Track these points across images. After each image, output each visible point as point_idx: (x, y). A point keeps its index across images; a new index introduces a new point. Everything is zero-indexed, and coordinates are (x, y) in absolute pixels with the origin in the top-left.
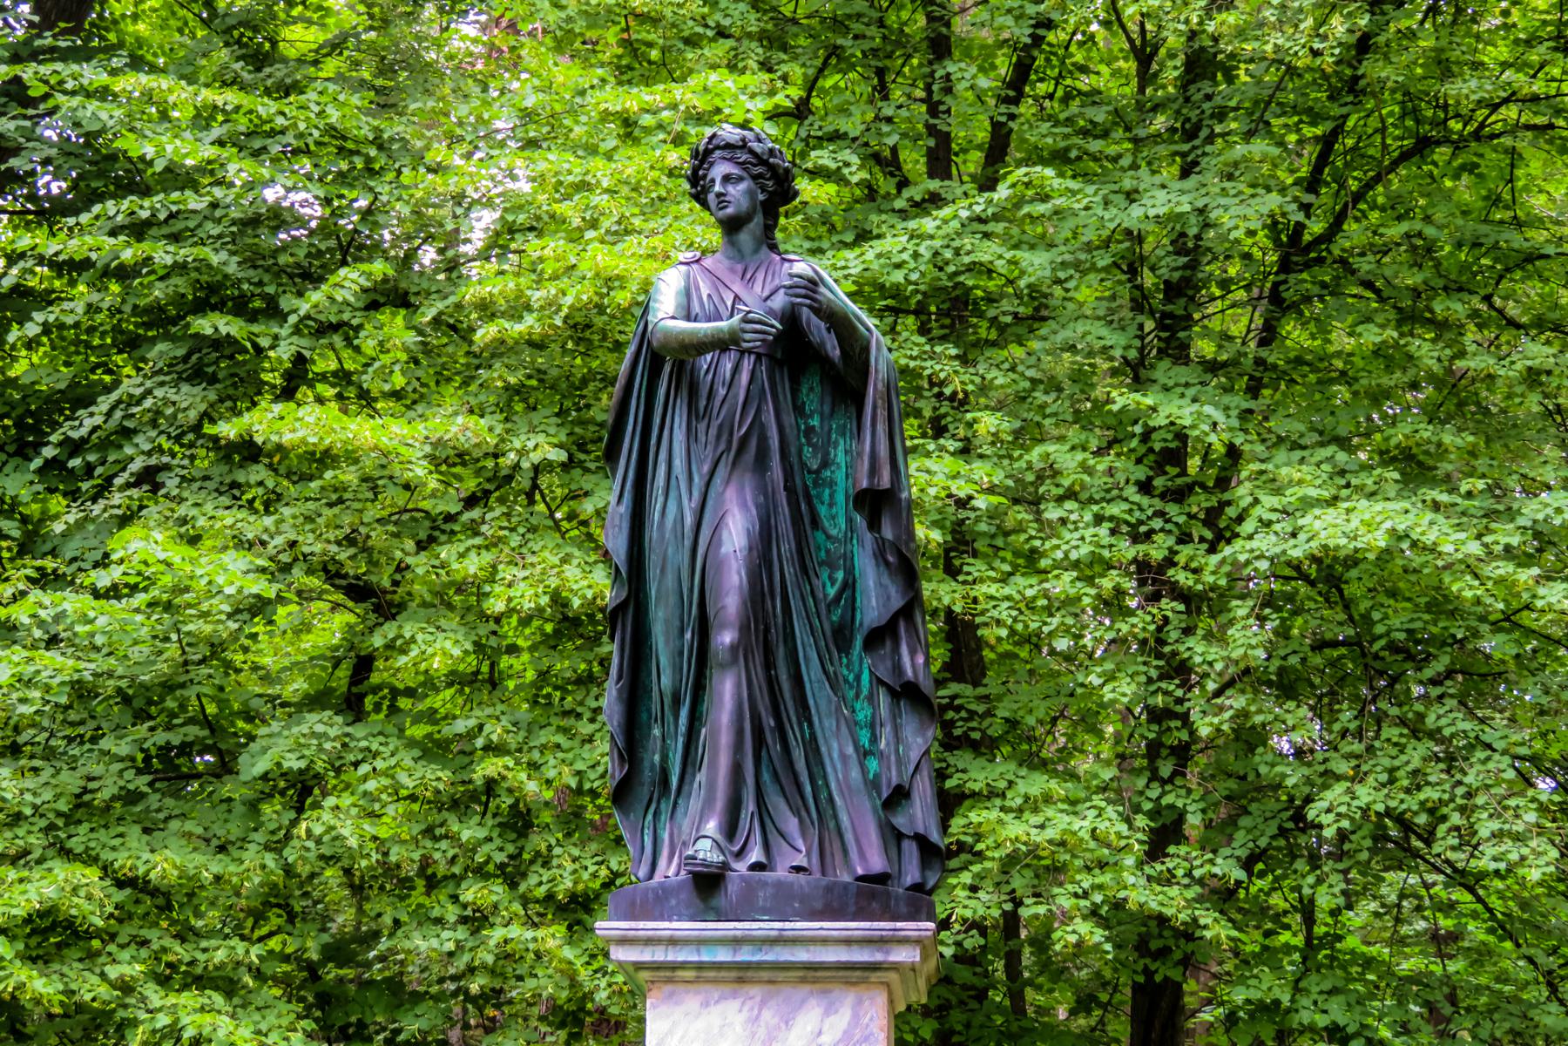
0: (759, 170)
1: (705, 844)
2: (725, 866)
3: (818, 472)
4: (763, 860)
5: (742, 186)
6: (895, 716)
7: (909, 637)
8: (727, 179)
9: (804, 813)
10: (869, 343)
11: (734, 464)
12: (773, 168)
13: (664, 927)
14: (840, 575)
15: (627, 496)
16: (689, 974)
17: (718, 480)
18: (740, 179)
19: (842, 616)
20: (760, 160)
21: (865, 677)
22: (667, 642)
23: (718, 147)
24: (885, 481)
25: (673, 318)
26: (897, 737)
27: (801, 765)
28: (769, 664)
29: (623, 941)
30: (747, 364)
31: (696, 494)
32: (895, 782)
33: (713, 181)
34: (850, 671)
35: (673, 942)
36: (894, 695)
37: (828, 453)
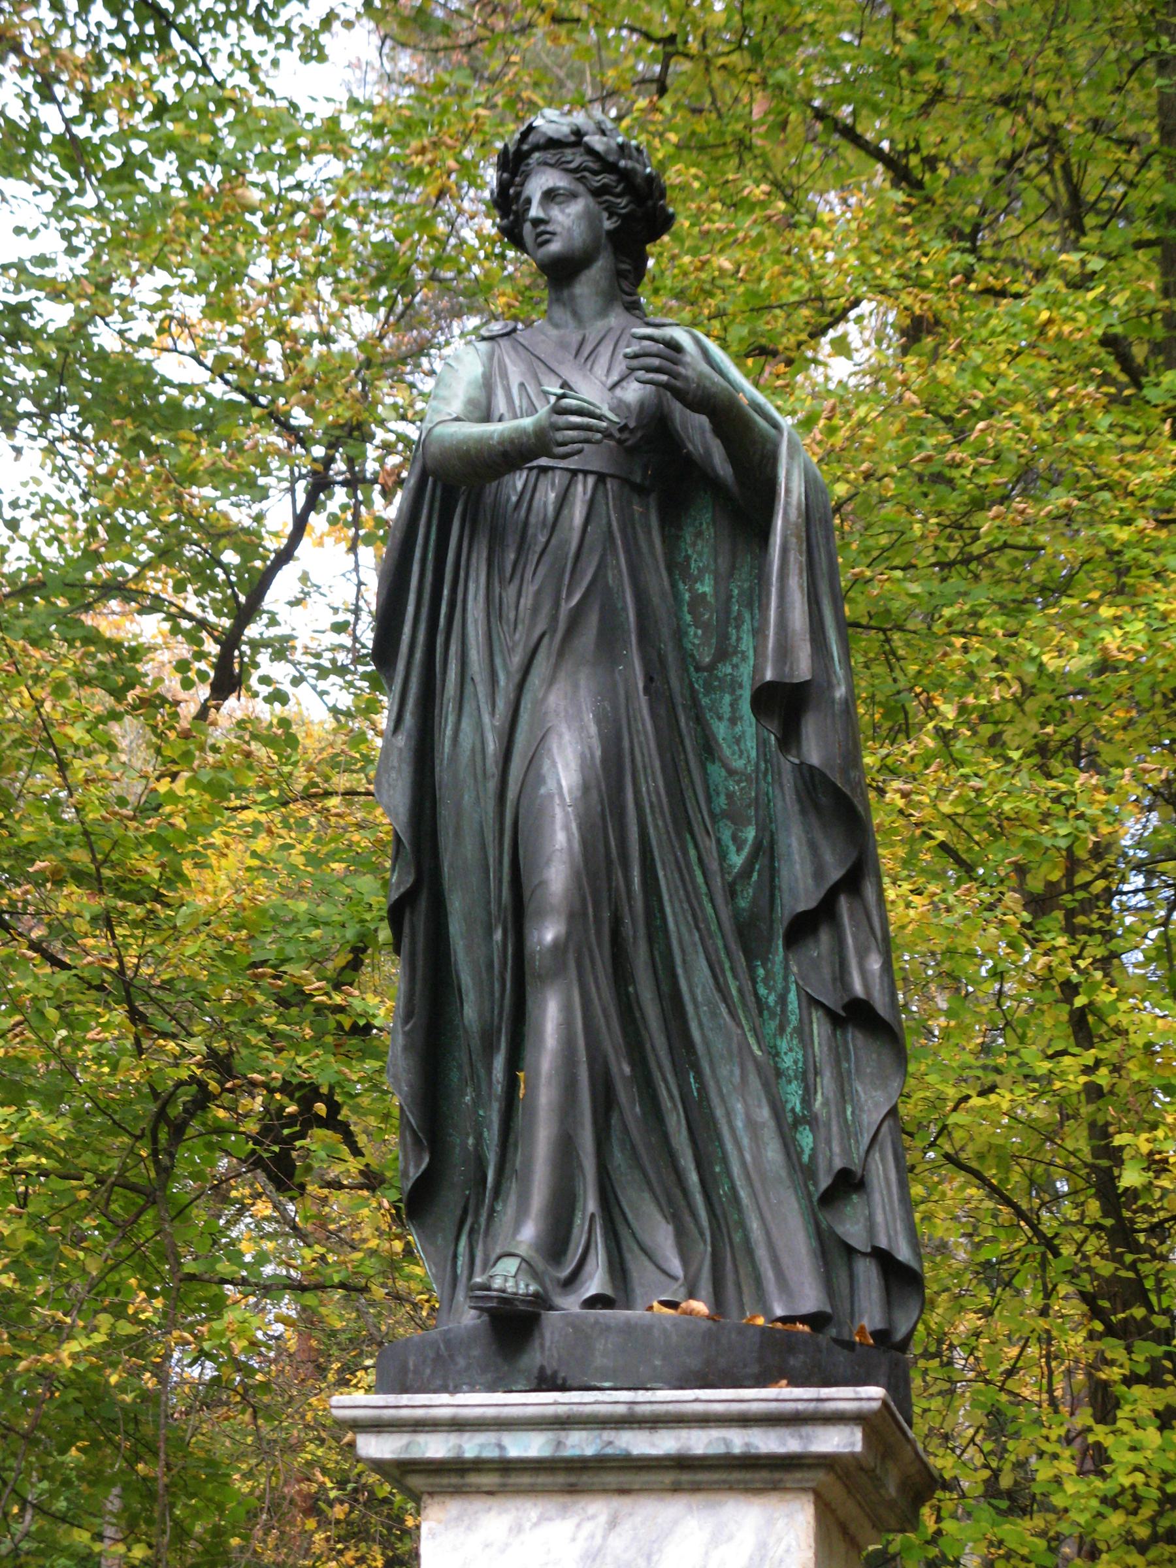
0: (598, 181)
1: (510, 1266)
2: (541, 1302)
3: (712, 667)
4: (609, 1292)
5: (576, 208)
6: (838, 1056)
7: (856, 925)
8: (550, 196)
9: (687, 1218)
10: (776, 446)
11: (561, 654)
12: (626, 176)
13: (442, 1404)
14: (750, 833)
15: (409, 720)
16: (488, 1480)
17: (536, 679)
18: (573, 196)
19: (754, 902)
20: (604, 163)
21: (792, 996)
22: (469, 948)
23: (537, 148)
24: (803, 668)
25: (457, 419)
26: (844, 1093)
27: (680, 1140)
28: (621, 974)
29: (377, 1426)
30: (582, 490)
31: (501, 704)
32: (838, 1164)
33: (528, 201)
34: (770, 989)
35: (458, 1425)
36: (835, 1020)
37: (725, 636)
